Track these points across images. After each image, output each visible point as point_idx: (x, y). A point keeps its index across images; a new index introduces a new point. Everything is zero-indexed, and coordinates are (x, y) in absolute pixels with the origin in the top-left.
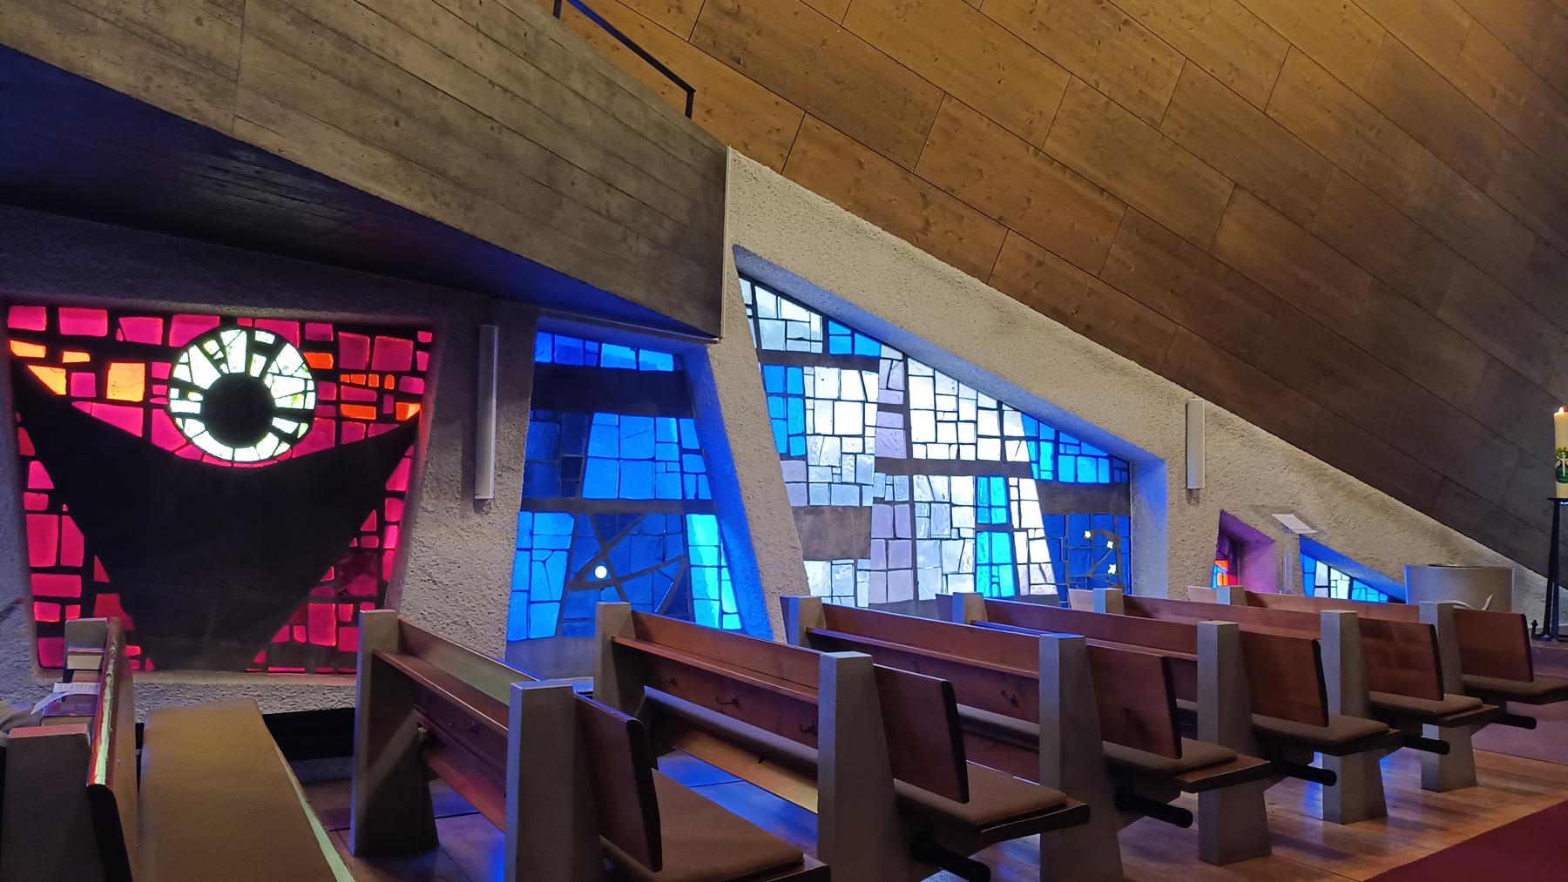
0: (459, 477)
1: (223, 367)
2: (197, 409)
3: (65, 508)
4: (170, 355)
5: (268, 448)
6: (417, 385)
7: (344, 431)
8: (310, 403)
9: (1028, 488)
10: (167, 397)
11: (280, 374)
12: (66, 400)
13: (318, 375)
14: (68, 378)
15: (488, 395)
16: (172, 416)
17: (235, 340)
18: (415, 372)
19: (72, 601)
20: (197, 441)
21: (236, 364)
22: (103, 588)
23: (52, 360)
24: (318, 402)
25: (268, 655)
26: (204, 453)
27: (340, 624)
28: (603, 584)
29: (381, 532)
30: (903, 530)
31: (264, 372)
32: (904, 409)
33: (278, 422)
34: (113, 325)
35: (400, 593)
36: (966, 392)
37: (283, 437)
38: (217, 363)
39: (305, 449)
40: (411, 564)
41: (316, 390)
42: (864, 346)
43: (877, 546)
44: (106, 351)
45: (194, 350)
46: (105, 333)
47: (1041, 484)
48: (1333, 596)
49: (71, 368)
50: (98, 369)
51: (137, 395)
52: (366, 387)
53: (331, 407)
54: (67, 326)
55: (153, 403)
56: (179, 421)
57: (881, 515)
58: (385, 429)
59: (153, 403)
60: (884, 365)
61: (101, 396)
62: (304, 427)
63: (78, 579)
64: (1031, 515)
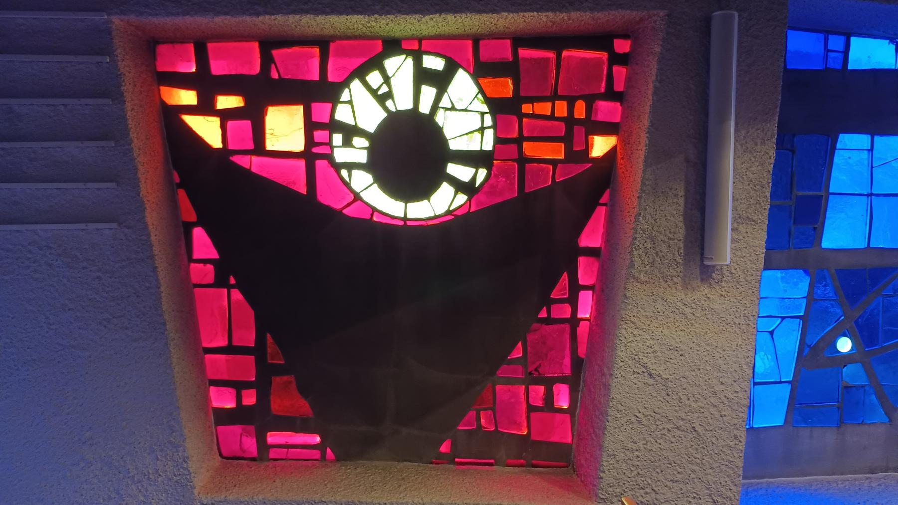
0: (681, 232)
1: (389, 104)
2: (362, 157)
3: (232, 281)
4: (330, 92)
5: (443, 201)
6: (607, 110)
7: (528, 177)
8: (488, 145)
10: (329, 144)
11: (453, 109)
12: (225, 151)
13: (497, 106)
14: (223, 127)
15: (723, 120)
16: (338, 167)
17: (400, 68)
18: (612, 95)
19: (247, 385)
20: (365, 196)
21: (403, 101)
22: (280, 370)
23: (205, 108)
24: (498, 141)
25: (454, 444)
26: (374, 210)
27: (531, 409)
28: (846, 359)
29: (573, 301)
31: (435, 107)
33: (455, 170)
34: (267, 60)
35: (607, 387)
37: (459, 186)
38: (382, 99)
39: (484, 200)
40: (621, 353)
41: (495, 126)
44: (262, 93)
45: (356, 84)
46: (257, 69)
48: (299, 110)
49: (226, 116)
50: (253, 114)
51: (297, 144)
52: (552, 117)
53: (513, 147)
54: (218, 68)
55: (315, 153)
56: (344, 173)
58: (577, 169)
59: (315, 153)
61: (259, 146)
62: (482, 173)
63: (251, 358)
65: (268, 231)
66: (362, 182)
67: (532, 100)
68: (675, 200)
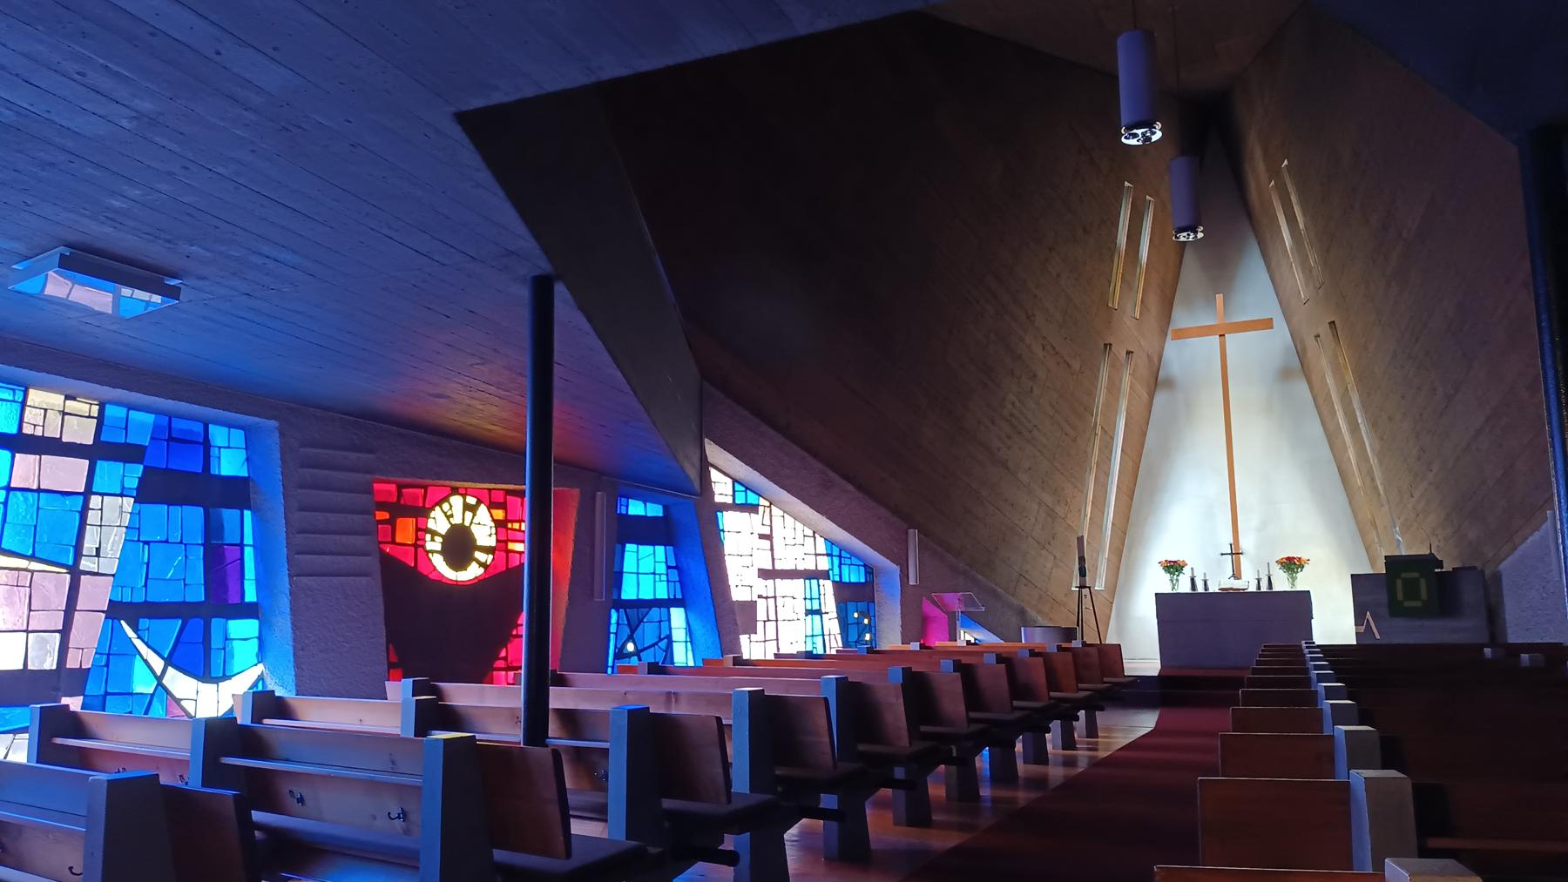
2: (438, 547)
9: (827, 586)
10: (424, 540)
21: (457, 520)
24: (498, 541)
30: (772, 617)
32: (769, 537)
33: (477, 555)
34: (400, 494)
36: (799, 526)
37: (481, 564)
38: (449, 517)
39: (492, 572)
42: (752, 498)
43: (760, 625)
47: (834, 582)
57: (761, 604)
59: (418, 545)
60: (761, 509)
64: (830, 605)
65: (404, 583)
66: (438, 562)
67: (513, 521)
68: (492, 705)
